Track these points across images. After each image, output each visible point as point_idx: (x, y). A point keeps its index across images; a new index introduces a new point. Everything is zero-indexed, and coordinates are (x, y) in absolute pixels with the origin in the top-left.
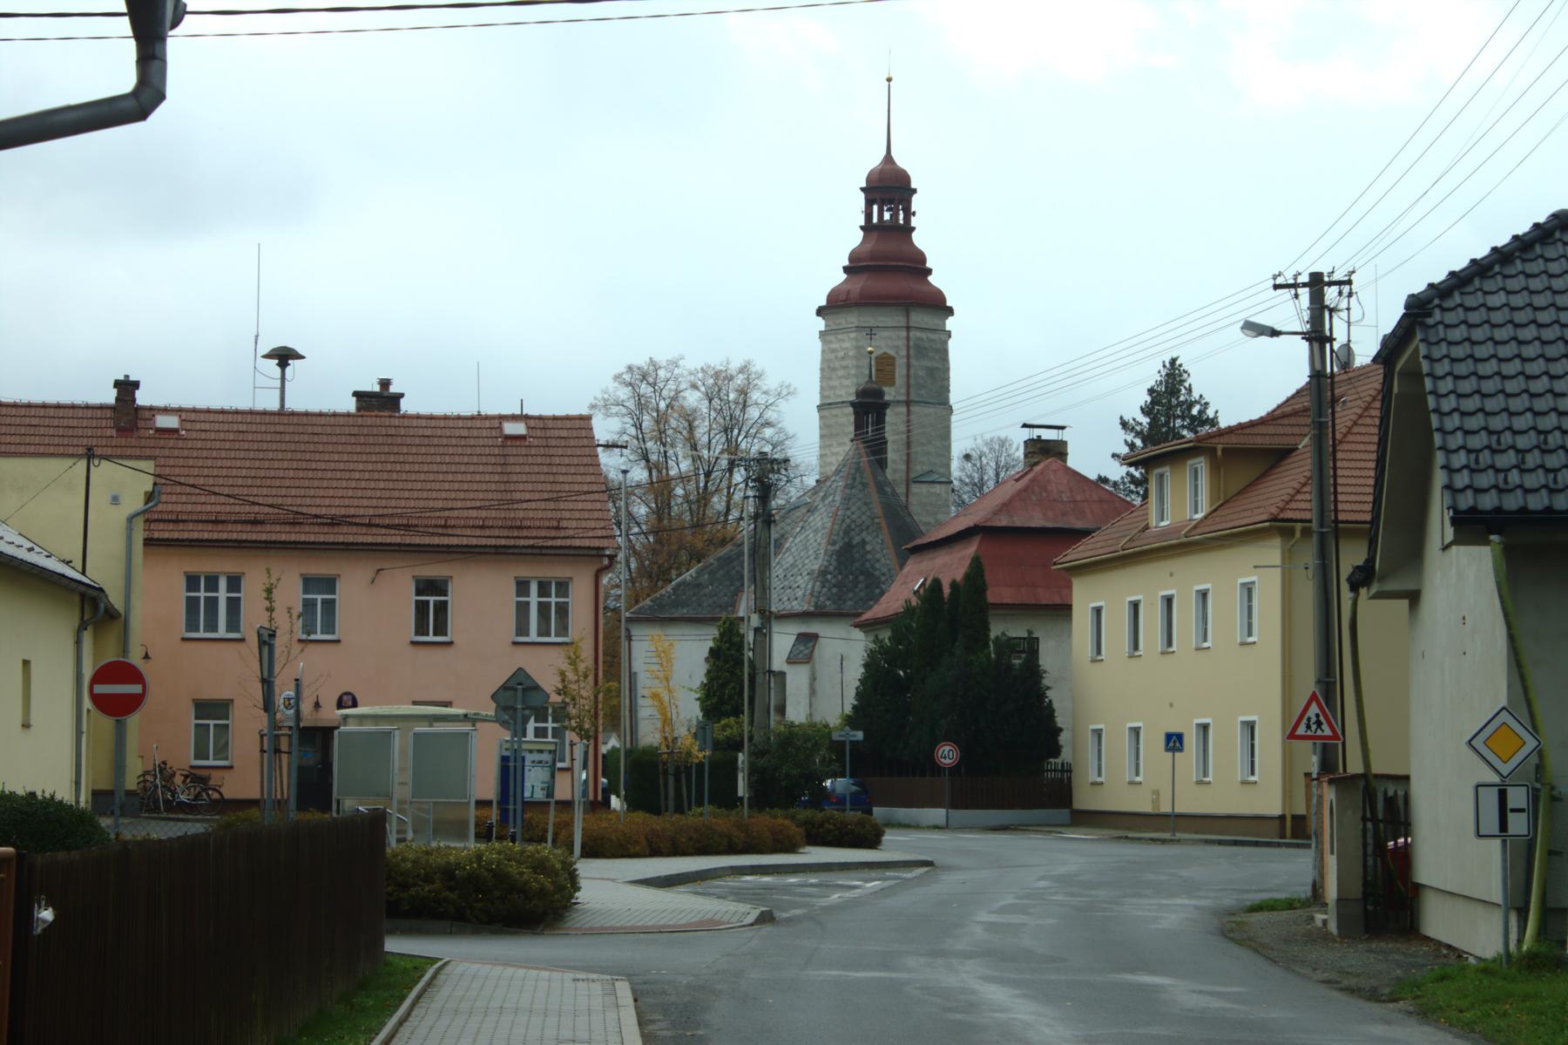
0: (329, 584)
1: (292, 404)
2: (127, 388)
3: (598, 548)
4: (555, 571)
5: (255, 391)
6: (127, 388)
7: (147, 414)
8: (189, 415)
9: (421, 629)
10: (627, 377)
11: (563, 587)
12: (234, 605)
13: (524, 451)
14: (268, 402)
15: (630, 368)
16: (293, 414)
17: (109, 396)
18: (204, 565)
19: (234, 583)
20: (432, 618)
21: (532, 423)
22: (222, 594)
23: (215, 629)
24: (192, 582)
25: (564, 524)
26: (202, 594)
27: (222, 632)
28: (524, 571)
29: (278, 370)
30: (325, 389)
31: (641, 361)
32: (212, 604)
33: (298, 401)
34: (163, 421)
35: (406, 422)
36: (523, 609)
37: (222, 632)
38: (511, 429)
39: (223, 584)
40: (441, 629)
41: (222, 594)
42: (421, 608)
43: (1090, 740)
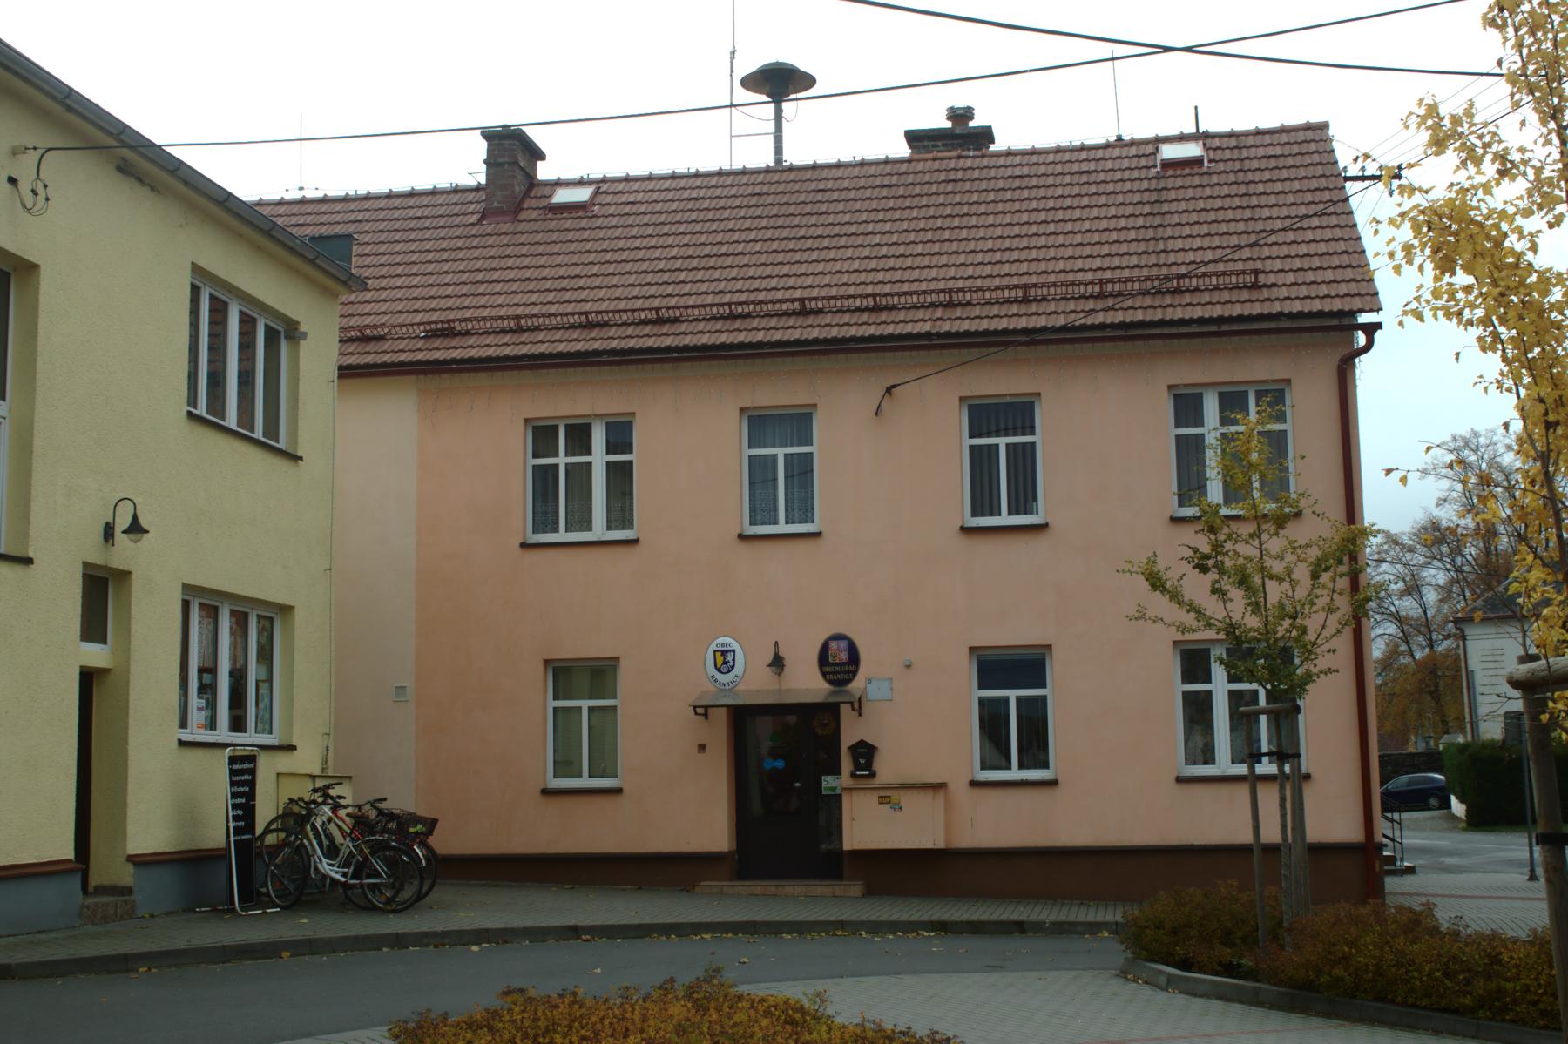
0: (797, 424)
1: (792, 156)
2: (511, 149)
3: (1341, 314)
4: (1256, 367)
5: (737, 141)
6: (511, 149)
7: (546, 191)
8: (601, 185)
9: (983, 501)
10: (1452, 445)
11: (1274, 396)
12: (621, 476)
13: (1197, 181)
14: (761, 157)
15: (1454, 439)
16: (792, 169)
17: (466, 165)
18: (565, 401)
19: (620, 438)
20: (1003, 482)
21: (1209, 142)
22: (599, 458)
23: (587, 525)
24: (543, 437)
25: (1262, 278)
26: (562, 460)
27: (599, 529)
28: (1187, 373)
29: (770, 108)
30: (849, 128)
31: (1464, 431)
32: (579, 476)
33: (798, 153)
34: (562, 196)
35: (993, 162)
36: (1190, 451)
37: (599, 529)
38: (1169, 152)
39: (599, 438)
40: (1024, 498)
41: (599, 458)
42: (982, 461)
43: (1540, 871)
